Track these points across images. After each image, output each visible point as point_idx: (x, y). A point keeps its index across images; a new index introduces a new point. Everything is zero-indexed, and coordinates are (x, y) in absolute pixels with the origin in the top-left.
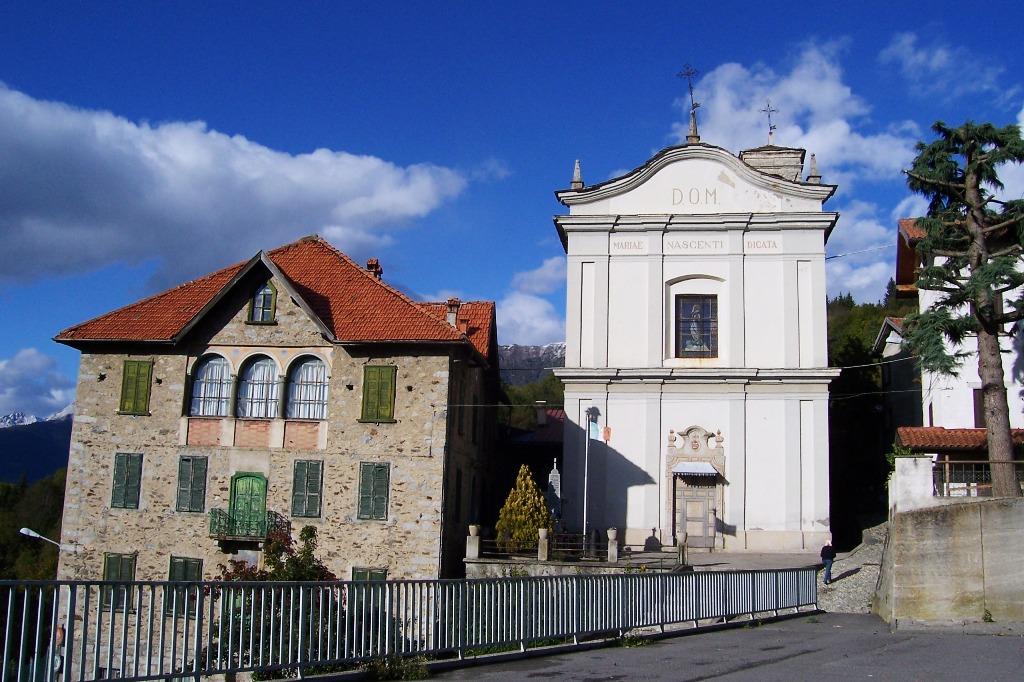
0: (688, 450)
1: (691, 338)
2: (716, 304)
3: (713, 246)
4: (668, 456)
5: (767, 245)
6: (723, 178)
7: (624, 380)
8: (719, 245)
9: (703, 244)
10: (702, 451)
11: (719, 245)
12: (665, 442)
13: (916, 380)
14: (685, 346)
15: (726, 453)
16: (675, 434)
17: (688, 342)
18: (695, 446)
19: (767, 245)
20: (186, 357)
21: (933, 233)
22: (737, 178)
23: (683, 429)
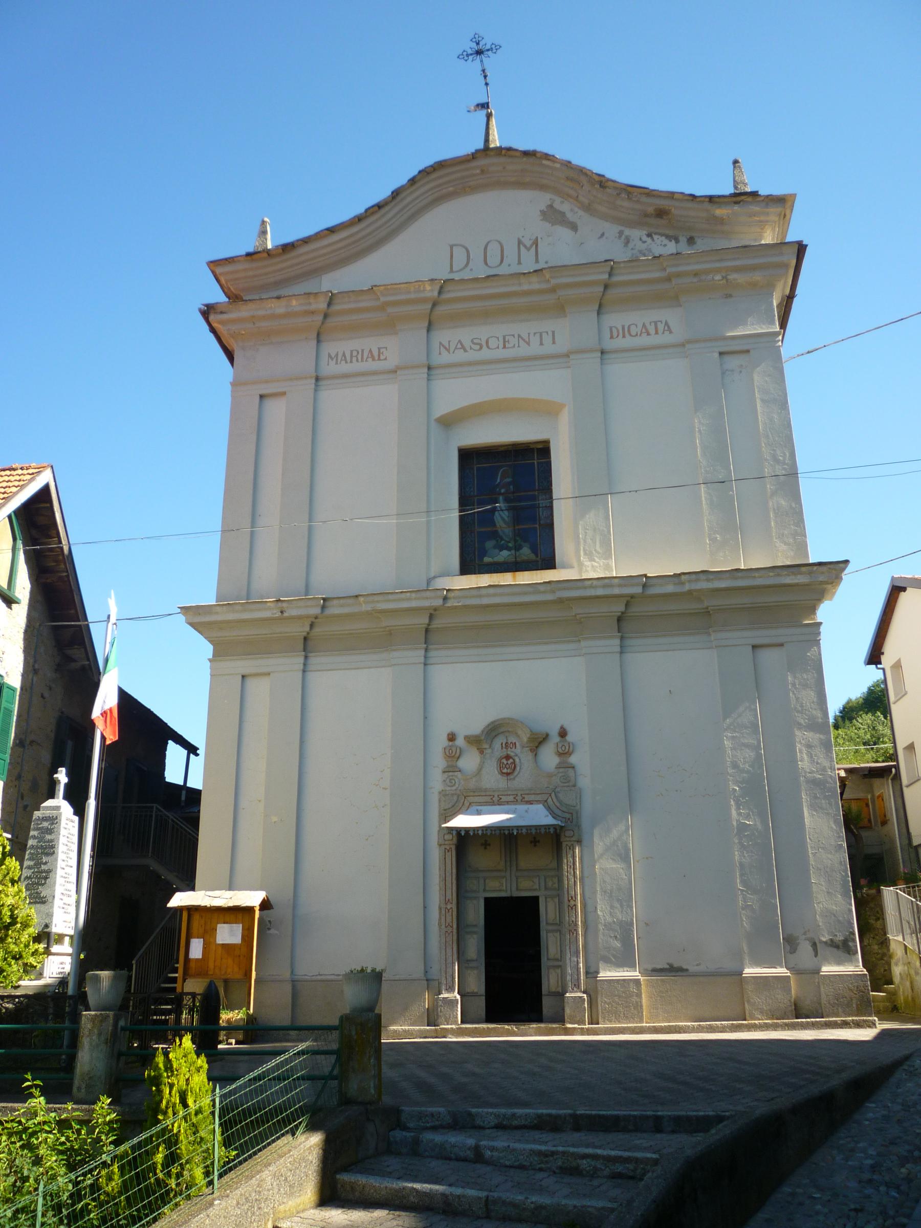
0: (492, 779)
1: (494, 535)
2: (549, 464)
3: (535, 341)
4: (443, 794)
5: (652, 330)
6: (552, 215)
7: (443, 951)
8: (547, 339)
9: (513, 341)
10: (524, 778)
11: (547, 339)
12: (438, 762)
13: (480, 832)
14: (484, 553)
15: (585, 782)
16: (460, 742)
17: (489, 544)
18: (508, 767)
19: (652, 330)
20: (188, 785)
21: (62, 1173)
22: (581, 213)
23: (477, 727)
